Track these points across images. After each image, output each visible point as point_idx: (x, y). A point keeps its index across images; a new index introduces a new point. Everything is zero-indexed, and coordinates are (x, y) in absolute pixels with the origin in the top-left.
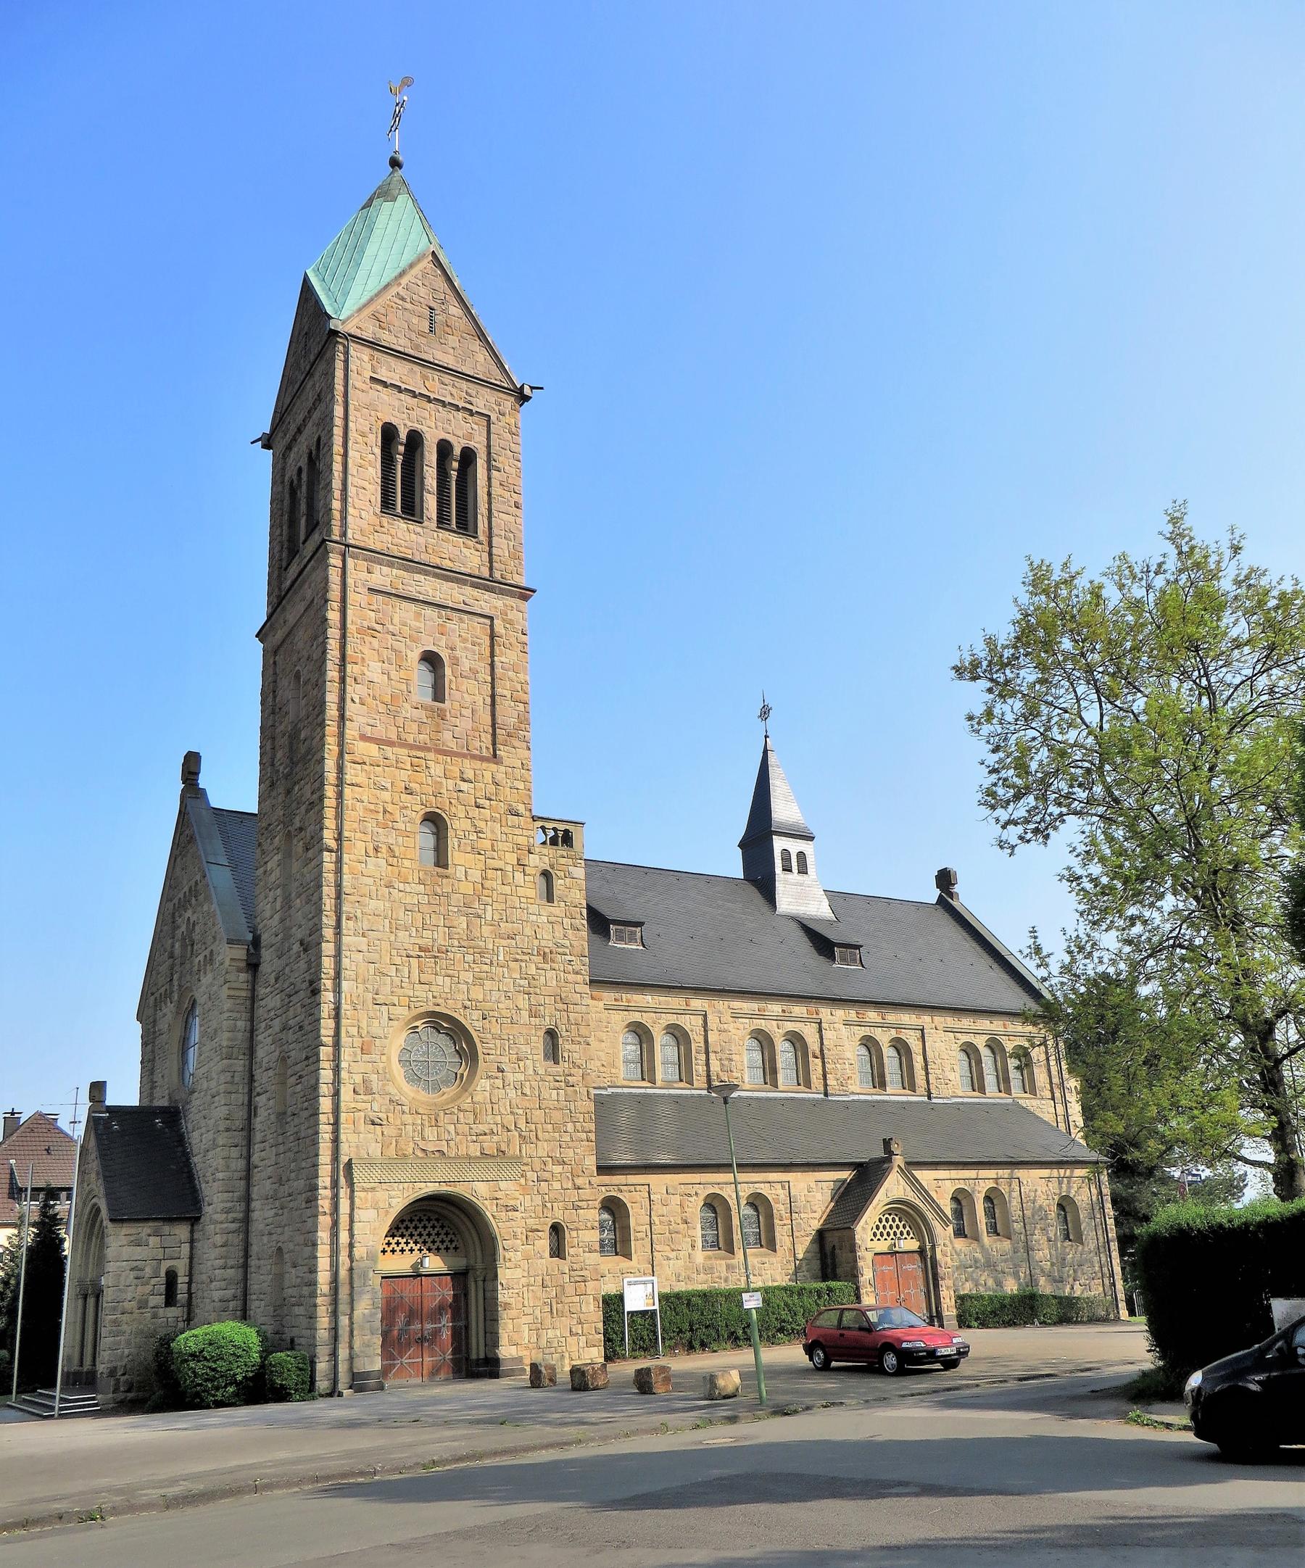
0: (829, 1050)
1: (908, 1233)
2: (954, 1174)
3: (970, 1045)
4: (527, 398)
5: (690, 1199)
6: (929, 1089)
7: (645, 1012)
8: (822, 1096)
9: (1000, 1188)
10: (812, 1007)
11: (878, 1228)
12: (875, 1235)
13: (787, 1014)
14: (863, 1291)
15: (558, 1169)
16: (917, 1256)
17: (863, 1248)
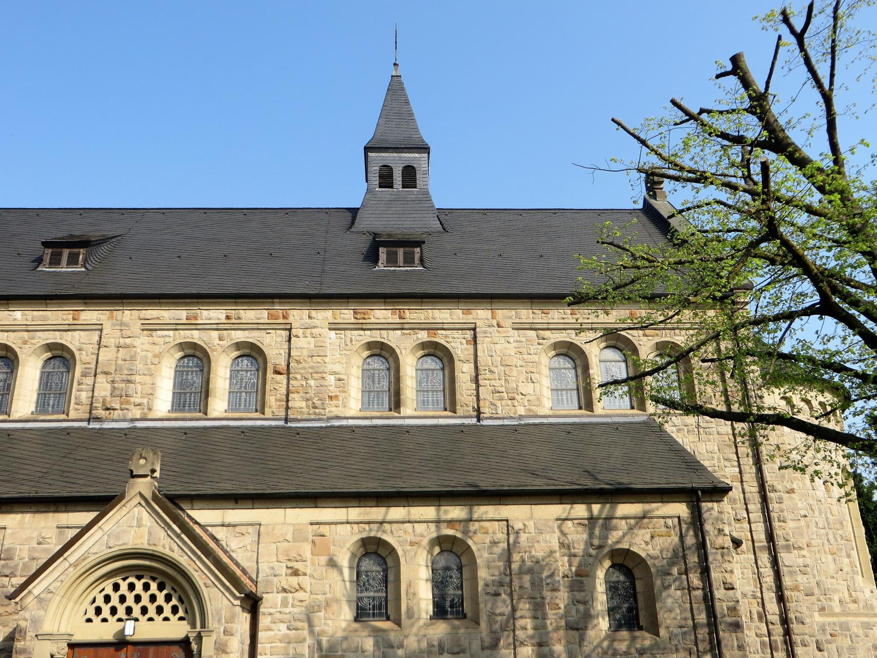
0: (298, 362)
1: (175, 610)
2: (355, 513)
3: (571, 346)
4: (872, 157)
6: (479, 408)
7: (14, 331)
9: (470, 542)
10: (279, 308)
11: (107, 599)
12: (98, 611)
13: (234, 321)
17: (30, 634)
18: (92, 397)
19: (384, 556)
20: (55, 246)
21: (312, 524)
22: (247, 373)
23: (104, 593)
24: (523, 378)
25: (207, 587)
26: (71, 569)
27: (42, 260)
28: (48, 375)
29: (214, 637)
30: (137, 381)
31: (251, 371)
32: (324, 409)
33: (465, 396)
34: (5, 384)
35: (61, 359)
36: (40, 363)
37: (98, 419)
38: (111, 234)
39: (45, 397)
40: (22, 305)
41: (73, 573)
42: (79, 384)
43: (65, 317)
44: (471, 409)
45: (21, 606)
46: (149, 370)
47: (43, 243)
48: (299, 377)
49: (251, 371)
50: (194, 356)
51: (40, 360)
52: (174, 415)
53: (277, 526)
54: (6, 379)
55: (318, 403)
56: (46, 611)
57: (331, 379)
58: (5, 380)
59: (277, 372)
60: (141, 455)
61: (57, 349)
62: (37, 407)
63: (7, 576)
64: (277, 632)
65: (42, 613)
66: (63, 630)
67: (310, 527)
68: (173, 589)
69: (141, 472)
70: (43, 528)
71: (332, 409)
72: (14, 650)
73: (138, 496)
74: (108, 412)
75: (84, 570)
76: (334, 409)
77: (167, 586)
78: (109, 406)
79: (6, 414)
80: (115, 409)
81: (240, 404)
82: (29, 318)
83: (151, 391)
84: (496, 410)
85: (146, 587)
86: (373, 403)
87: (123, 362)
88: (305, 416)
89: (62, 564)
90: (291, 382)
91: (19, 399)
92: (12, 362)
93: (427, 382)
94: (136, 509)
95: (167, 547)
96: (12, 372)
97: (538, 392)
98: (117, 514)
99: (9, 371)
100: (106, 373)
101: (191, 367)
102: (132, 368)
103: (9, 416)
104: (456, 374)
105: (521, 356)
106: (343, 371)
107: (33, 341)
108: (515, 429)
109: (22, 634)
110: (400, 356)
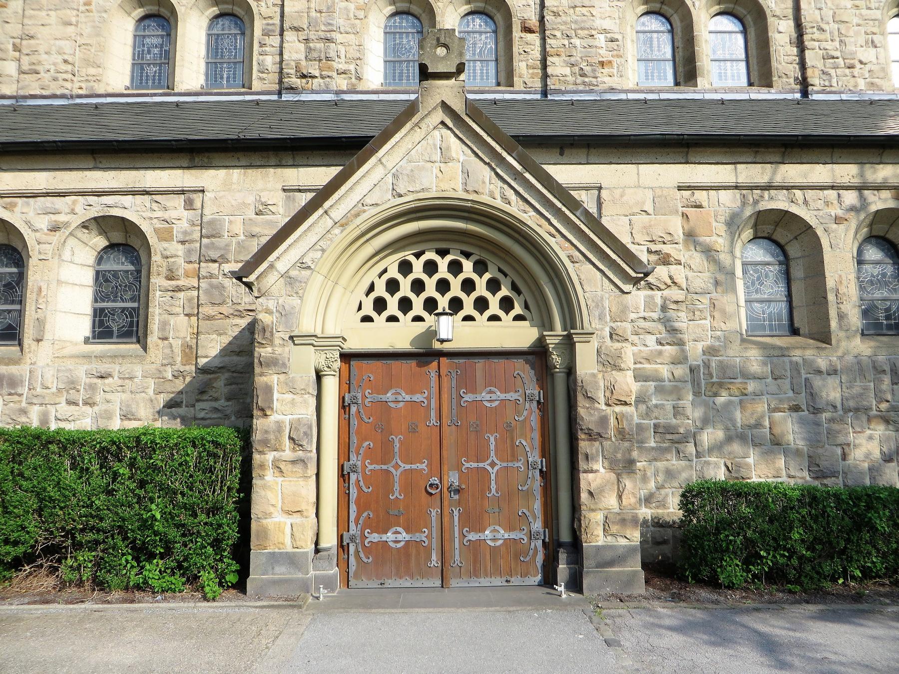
0: (556, 14)
1: (507, 305)
8: (538, 97)
11: (393, 286)
12: (380, 305)
14: (263, 458)
16: (524, 370)
17: (280, 336)
18: (281, 61)
19: (782, 242)
21: (680, 188)
22: (481, 35)
23: (386, 277)
24: (861, 40)
25: (573, 262)
26: (337, 231)
28: (217, 39)
29: (595, 343)
30: (338, 41)
31: (486, 33)
32: (596, 78)
33: (783, 64)
34: (161, 51)
35: (232, 18)
36: (204, 22)
37: (292, 89)
39: (216, 68)
41: (341, 237)
42: (262, 45)
44: (792, 80)
45: (259, 291)
46: (353, 26)
48: (558, 34)
49: (486, 33)
50: (408, 13)
53: (628, 191)
54: (162, 45)
55: (587, 69)
56: (301, 298)
57: (601, 40)
58: (162, 46)
59: (527, 30)
60: (438, 39)
62: (207, 80)
63: (215, 261)
64: (643, 348)
65: (295, 301)
66: (330, 331)
67: (679, 194)
68: (500, 270)
69: (441, 68)
70: (262, 190)
71: (605, 79)
72: (256, 361)
73: (440, 110)
74: (304, 81)
75: (358, 232)
76: (607, 79)
77: (490, 266)
78: (305, 73)
80: (315, 77)
81: (475, 76)
83: (358, 55)
84: (830, 81)
85: (455, 267)
86: (652, 76)
87: (318, 15)
88: (570, 87)
89: (321, 222)
90: (548, 41)
92: (167, 21)
93: (724, 47)
94: (436, 133)
95: (498, 196)
97: (882, 60)
98: (407, 139)
100: (297, 29)
101: (405, 28)
102: (331, 22)
104: (770, 34)
105: (858, 12)
106: (616, 29)
109: (268, 334)
110: (692, 9)
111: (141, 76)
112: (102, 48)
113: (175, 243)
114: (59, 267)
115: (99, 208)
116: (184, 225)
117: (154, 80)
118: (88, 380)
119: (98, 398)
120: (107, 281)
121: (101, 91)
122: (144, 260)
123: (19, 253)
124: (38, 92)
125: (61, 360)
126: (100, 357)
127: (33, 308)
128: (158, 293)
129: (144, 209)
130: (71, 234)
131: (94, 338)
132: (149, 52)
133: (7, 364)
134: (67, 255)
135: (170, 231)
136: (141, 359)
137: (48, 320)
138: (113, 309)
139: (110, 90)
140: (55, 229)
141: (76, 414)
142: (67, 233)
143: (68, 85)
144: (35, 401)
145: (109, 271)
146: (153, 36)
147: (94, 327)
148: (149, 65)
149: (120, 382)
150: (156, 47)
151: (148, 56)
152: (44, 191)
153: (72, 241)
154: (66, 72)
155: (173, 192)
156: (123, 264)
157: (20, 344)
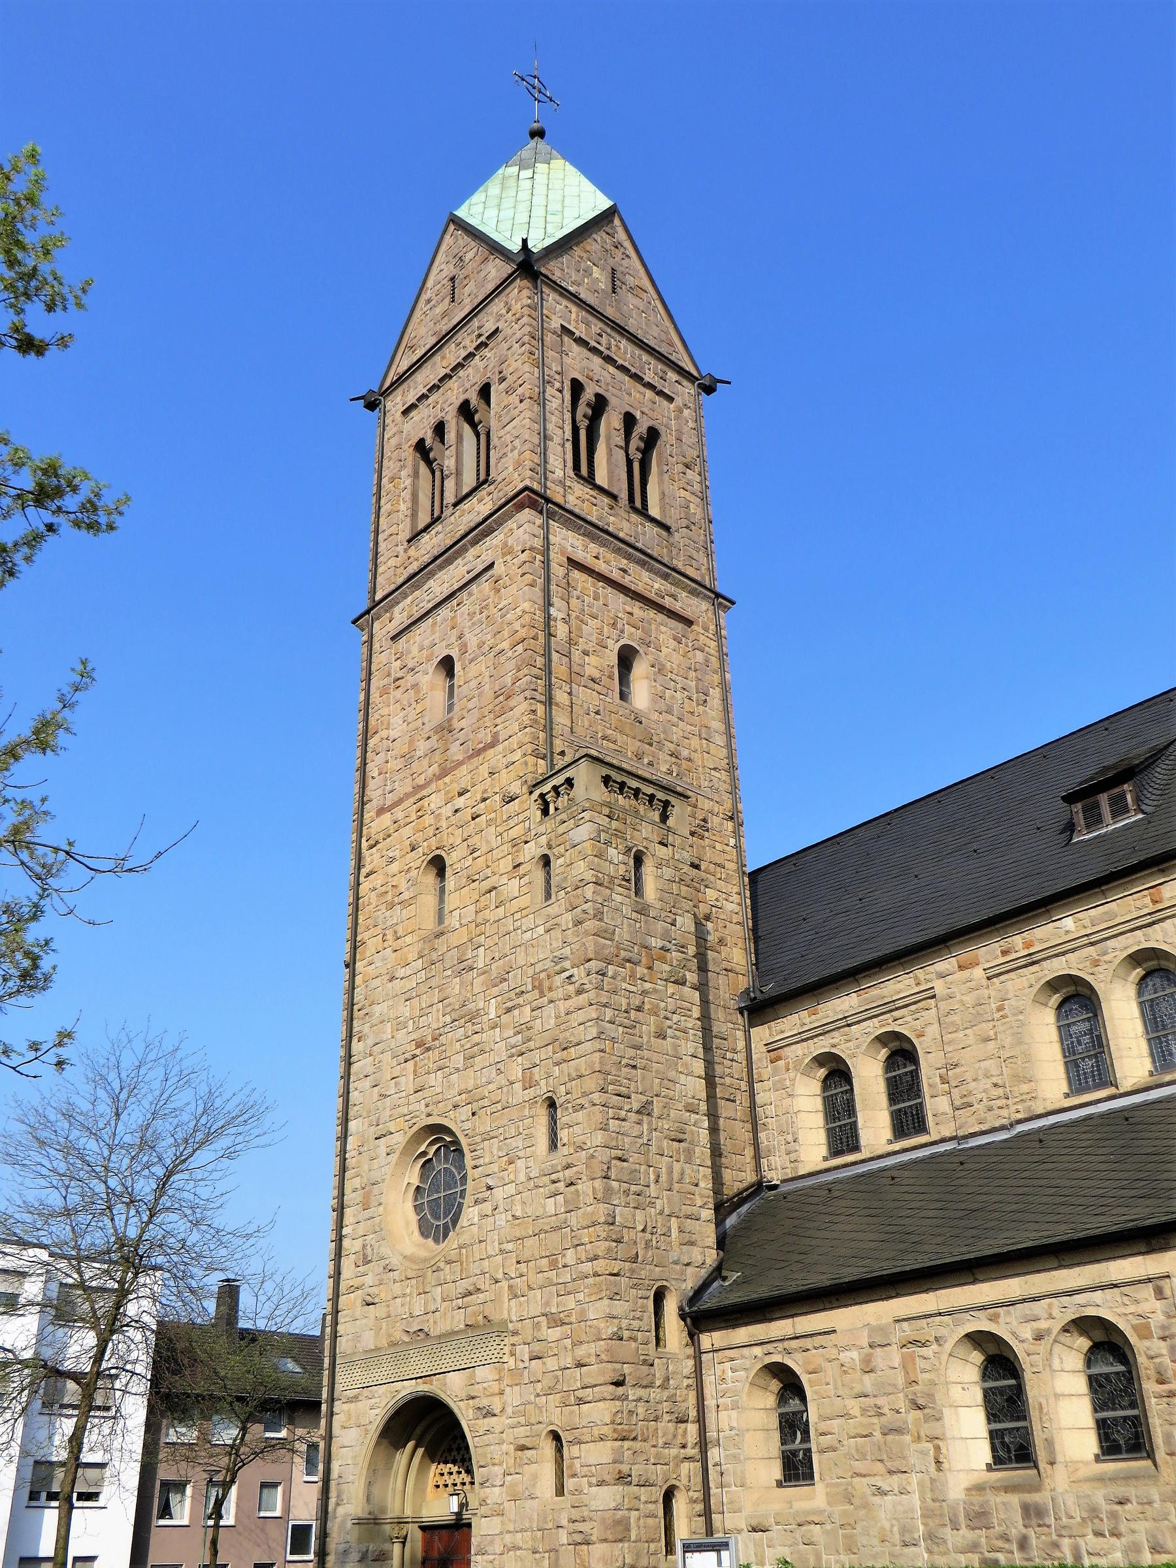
5: (924, 1351)
7: (1073, 950)
15: (554, 1333)
20: (1083, 795)
27: (1073, 825)
28: (1151, 1006)
34: (1092, 1038)
36: (1131, 990)
38: (1163, 741)
39: (1161, 1043)
40: (1067, 906)
43: (1139, 904)
47: (1063, 798)
51: (1129, 984)
52: (897, 1146)
54: (1091, 1029)
61: (1150, 959)
62: (1154, 1062)
79: (1112, 1085)
82: (1087, 922)
91: (1121, 1057)
92: (1089, 999)
96: (1096, 1015)
99: (1091, 1015)
103: (1117, 1088)
107: (1106, 958)
108: (1039, 1138)
111: (1078, 1076)
112: (1028, 1059)
113: (1156, 1340)
114: (1052, 1379)
115: (1073, 1309)
116: (1160, 1317)
117: (1093, 1076)
118: (1108, 1507)
119: (1123, 1527)
120: (1101, 1386)
121: (1040, 1111)
122: (1131, 1361)
123: (1013, 1364)
124: (976, 1129)
125: (1076, 1485)
126: (1114, 1479)
127: (1040, 1428)
128: (1153, 1400)
129: (1116, 1304)
130: (1055, 1341)
131: (1103, 1454)
132: (1079, 1043)
133: (1029, 1492)
134: (1056, 1364)
135: (1147, 1327)
136: (1154, 1478)
137: (1056, 1440)
138: (1115, 1419)
139: (1050, 1108)
140: (1039, 1337)
141: (1105, 1546)
142: (1051, 1341)
143: (1004, 1113)
144: (1064, 1533)
145: (1101, 1375)
146: (1079, 1021)
147: (1101, 1442)
148: (1083, 1059)
149: (1139, 1508)
150: (1085, 1034)
151: (1080, 1048)
152: (1020, 1298)
153: (1058, 1348)
154: (999, 1098)
155: (1140, 1282)
156: (1112, 1364)
157: (1036, 1467)
